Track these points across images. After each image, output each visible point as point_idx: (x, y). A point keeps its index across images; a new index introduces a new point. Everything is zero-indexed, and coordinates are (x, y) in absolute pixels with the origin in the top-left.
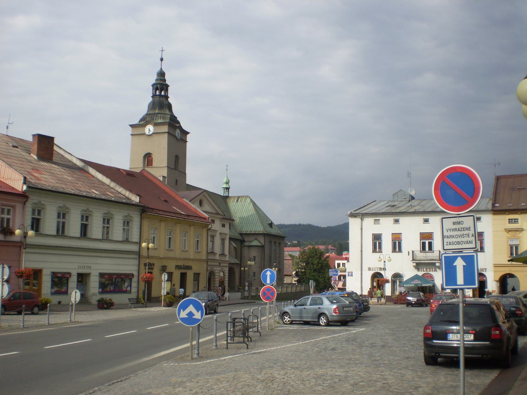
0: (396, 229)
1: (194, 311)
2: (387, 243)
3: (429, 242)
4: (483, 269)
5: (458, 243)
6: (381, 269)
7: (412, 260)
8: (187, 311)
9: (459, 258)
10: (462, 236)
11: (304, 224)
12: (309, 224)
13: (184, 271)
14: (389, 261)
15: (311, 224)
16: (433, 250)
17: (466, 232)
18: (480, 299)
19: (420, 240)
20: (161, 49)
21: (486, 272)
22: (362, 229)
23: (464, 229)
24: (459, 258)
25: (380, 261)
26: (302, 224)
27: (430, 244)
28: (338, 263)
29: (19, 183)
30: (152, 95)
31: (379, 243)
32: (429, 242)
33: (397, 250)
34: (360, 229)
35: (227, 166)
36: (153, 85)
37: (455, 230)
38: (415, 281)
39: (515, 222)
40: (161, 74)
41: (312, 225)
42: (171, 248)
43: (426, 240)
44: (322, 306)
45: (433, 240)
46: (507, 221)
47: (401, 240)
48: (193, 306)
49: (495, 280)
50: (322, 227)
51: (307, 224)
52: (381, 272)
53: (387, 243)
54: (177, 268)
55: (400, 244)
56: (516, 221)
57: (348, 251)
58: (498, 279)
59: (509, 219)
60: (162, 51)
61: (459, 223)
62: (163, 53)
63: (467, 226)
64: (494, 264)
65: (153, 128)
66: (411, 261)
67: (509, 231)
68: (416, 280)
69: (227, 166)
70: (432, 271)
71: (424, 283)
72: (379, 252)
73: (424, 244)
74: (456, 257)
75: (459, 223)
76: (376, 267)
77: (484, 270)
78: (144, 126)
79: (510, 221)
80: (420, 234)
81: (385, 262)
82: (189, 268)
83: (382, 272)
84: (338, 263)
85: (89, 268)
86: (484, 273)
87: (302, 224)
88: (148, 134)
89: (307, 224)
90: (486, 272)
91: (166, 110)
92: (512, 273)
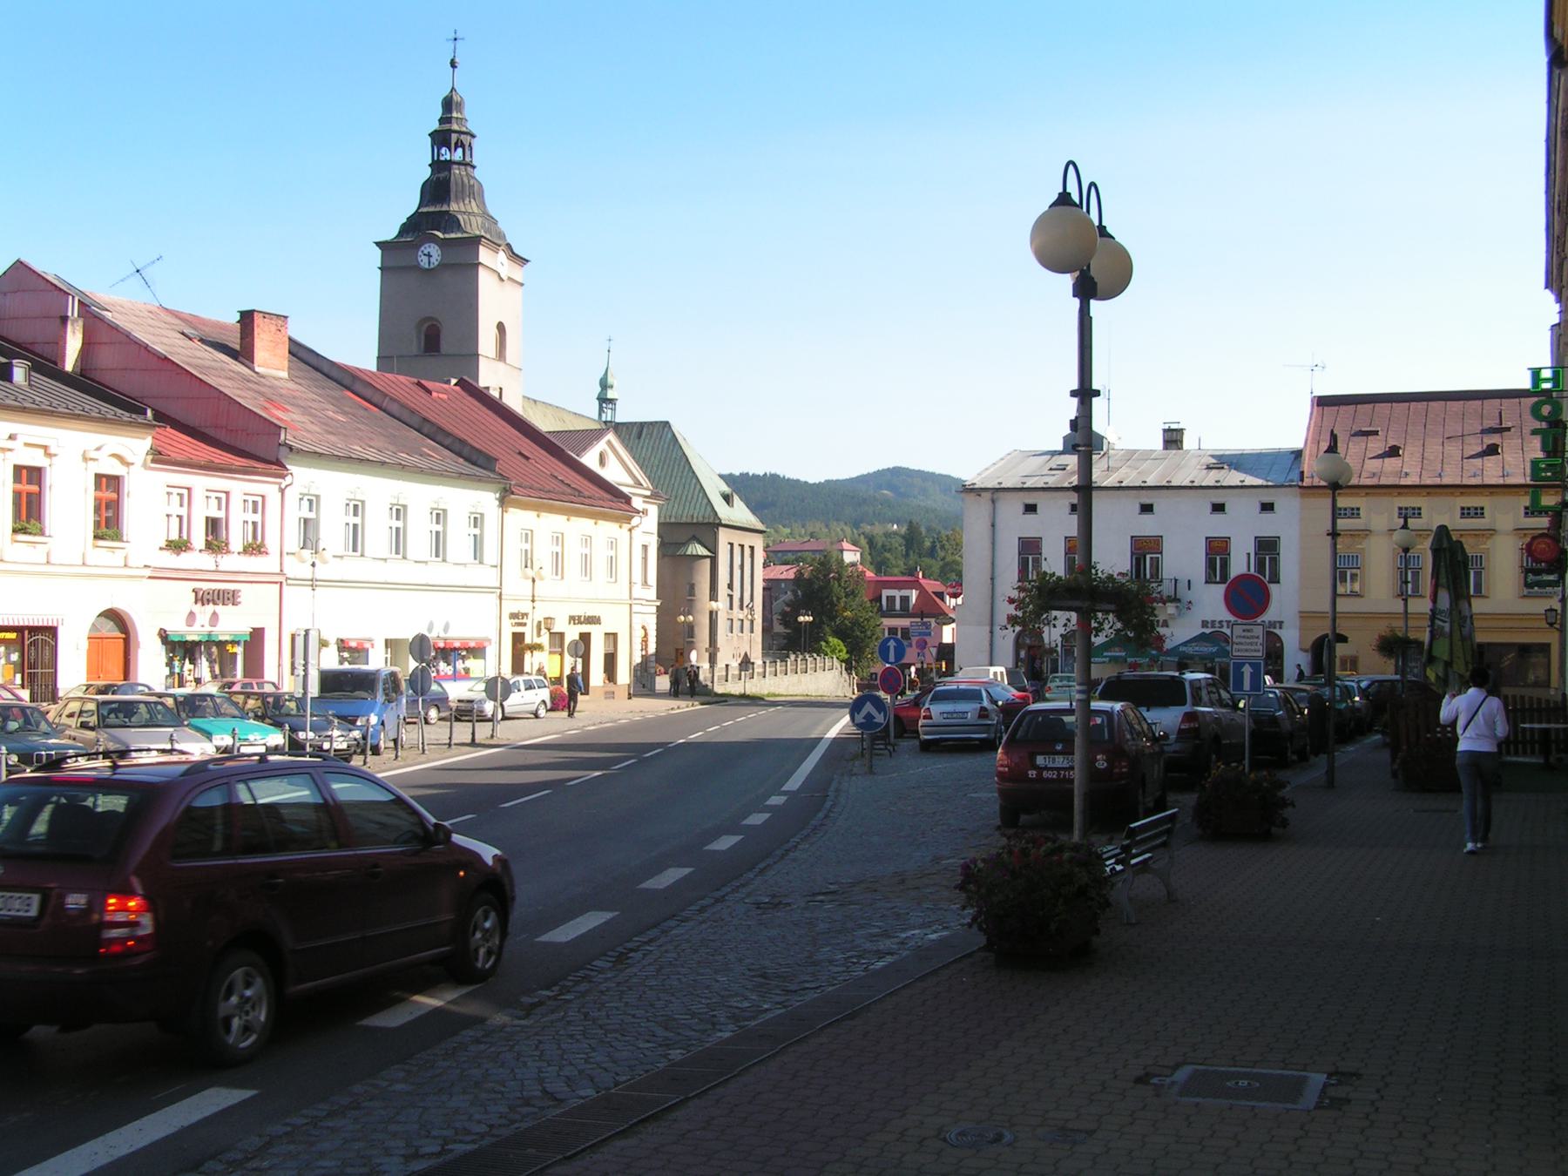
1: (874, 712)
4: (1275, 622)
5: (1246, 650)
8: (864, 712)
9: (1247, 665)
10: (1251, 644)
11: (757, 473)
12: (773, 472)
13: (585, 628)
15: (778, 473)
17: (1256, 640)
20: (452, 36)
21: (1281, 628)
23: (1252, 637)
24: (1247, 665)
26: (751, 474)
28: (887, 597)
29: (35, 380)
30: (430, 162)
34: (990, 524)
35: (610, 340)
36: (432, 135)
37: (1244, 637)
38: (1112, 649)
39: (1476, 514)
40: (449, 104)
41: (779, 476)
45: (1161, 553)
48: (873, 705)
49: (1301, 649)
50: (811, 481)
51: (766, 474)
54: (572, 622)
57: (254, 311)
58: (1308, 645)
60: (455, 39)
61: (1248, 631)
62: (457, 46)
63: (1256, 635)
64: (1300, 612)
65: (439, 252)
68: (1117, 649)
69: (610, 340)
74: (1244, 664)
75: (1248, 631)
77: (1278, 625)
78: (416, 246)
80: (1132, 540)
82: (593, 620)
84: (887, 597)
86: (1277, 631)
87: (751, 474)
88: (427, 266)
89: (766, 474)
90: (1281, 628)
91: (470, 202)
92: (1344, 634)
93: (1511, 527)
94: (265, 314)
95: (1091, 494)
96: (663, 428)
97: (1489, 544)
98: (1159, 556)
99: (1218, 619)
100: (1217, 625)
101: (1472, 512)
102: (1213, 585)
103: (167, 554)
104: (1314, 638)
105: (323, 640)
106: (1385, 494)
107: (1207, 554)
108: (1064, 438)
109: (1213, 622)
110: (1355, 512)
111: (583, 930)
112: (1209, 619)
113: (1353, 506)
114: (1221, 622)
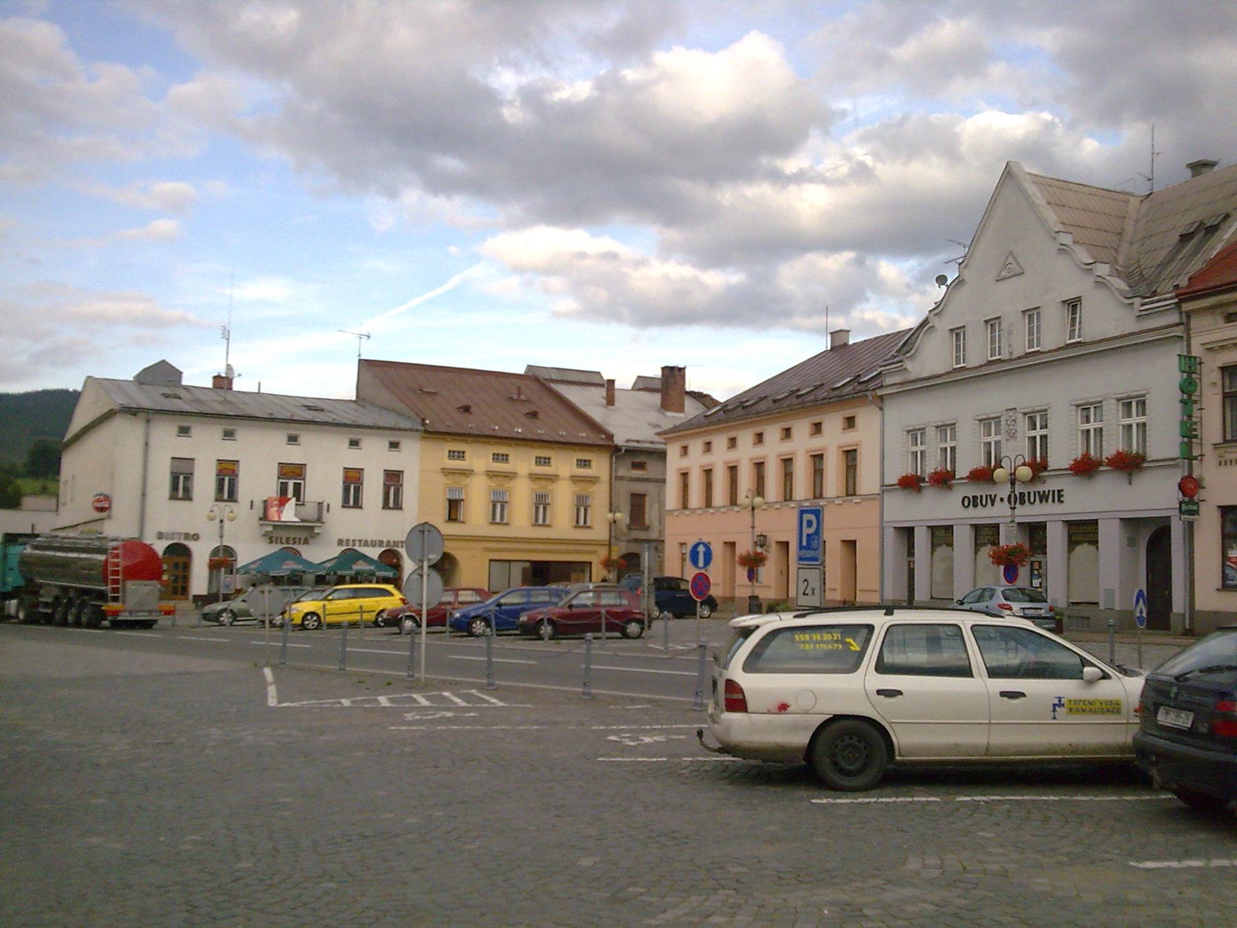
0: (228, 451)
2: (204, 482)
3: (295, 483)
4: (398, 542)
6: (187, 536)
7: (1220, 587)
14: (232, 520)
16: (302, 500)
18: (751, 619)
19: (279, 478)
22: (147, 444)
25: (212, 519)
27: (297, 488)
31: (230, 480)
32: (295, 483)
33: (180, 494)
39: (459, 456)
42: (505, 521)
43: (289, 479)
44: (873, 668)
45: (304, 479)
46: (534, 460)
47: (237, 476)
52: (186, 543)
53: (204, 482)
55: (358, 491)
56: (461, 455)
59: (494, 454)
66: (1218, 590)
67: (447, 472)
70: (299, 543)
71: (378, 570)
72: (184, 499)
73: (283, 489)
76: (176, 532)
79: (453, 455)
81: (221, 521)
83: (191, 545)
85: (120, 594)
93: (484, 470)
94: (1068, 597)
95: (357, 396)
96: (1181, 236)
97: (468, 481)
98: (302, 482)
99: (352, 538)
100: (351, 543)
101: (500, 457)
102: (177, 502)
103: (657, 436)
104: (213, 548)
105: (990, 667)
106: (484, 442)
107: (344, 483)
108: (163, 361)
109: (348, 540)
110: (461, 455)
111: (869, 648)
112: (344, 538)
113: (504, 453)
114: (354, 541)
